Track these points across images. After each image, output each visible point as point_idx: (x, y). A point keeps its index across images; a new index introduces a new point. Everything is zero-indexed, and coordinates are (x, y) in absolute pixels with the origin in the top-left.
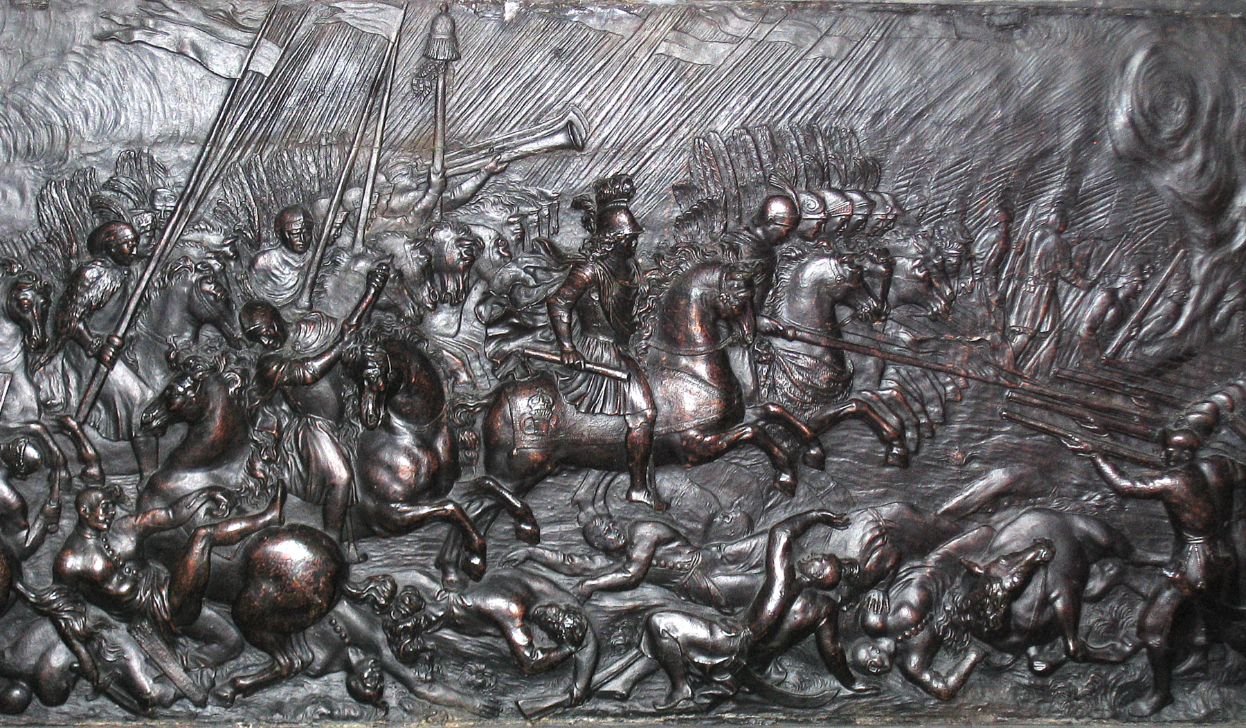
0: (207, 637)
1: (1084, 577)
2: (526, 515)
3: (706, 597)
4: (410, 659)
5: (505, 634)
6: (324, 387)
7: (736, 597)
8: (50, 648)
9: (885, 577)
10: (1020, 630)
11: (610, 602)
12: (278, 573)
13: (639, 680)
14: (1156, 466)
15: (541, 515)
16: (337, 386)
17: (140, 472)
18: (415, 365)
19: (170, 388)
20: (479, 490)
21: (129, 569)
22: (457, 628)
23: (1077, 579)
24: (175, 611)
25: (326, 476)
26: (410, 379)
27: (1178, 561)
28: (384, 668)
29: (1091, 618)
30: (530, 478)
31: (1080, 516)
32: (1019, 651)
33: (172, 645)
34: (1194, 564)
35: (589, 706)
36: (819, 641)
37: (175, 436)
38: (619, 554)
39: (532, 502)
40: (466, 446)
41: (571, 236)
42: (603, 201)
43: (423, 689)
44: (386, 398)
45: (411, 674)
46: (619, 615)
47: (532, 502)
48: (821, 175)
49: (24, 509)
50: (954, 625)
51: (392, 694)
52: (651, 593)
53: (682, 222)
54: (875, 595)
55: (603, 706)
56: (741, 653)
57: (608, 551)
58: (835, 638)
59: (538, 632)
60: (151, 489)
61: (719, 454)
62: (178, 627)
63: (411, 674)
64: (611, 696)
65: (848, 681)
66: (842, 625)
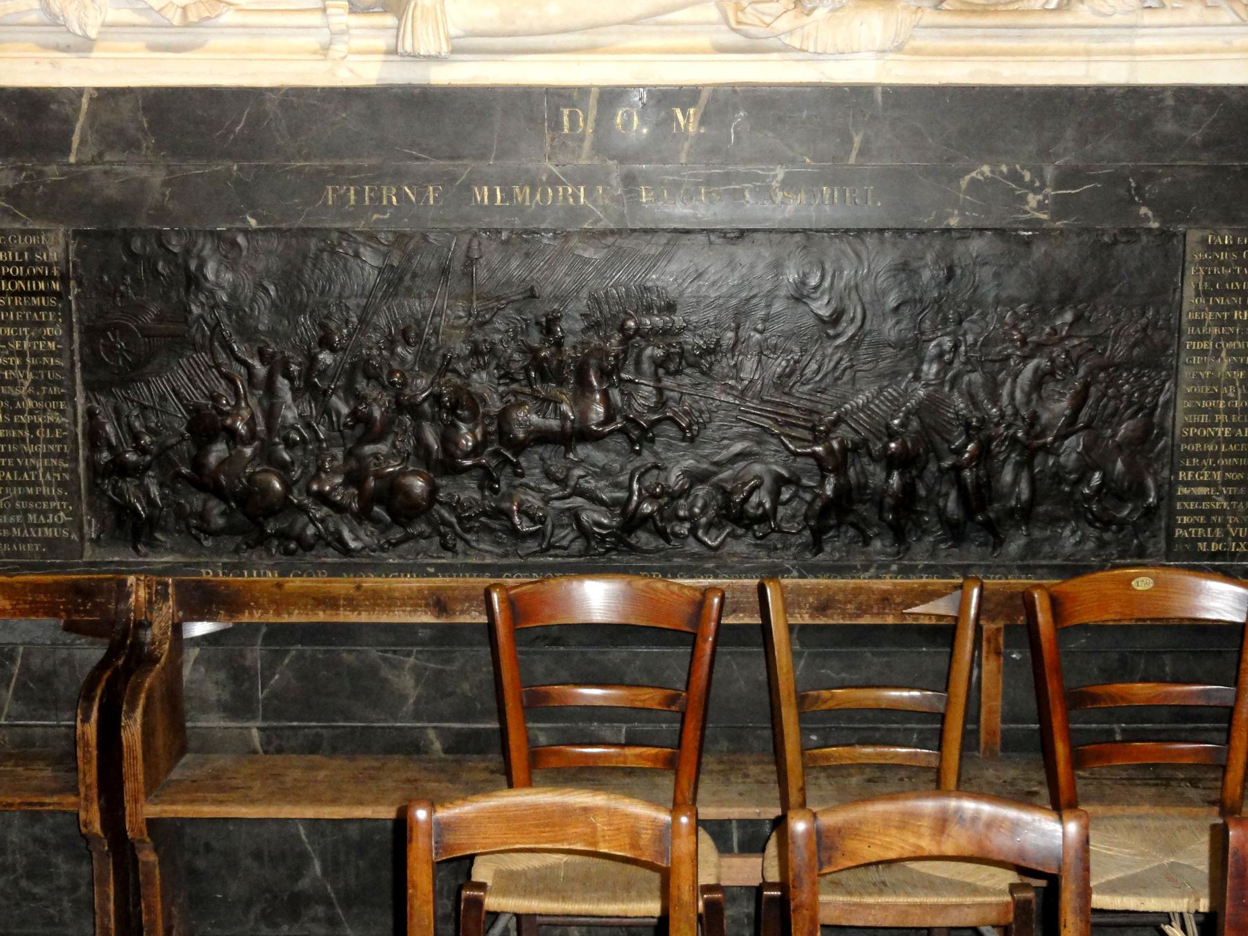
0: (376, 521)
1: (779, 493)
2: (517, 465)
3: (601, 502)
4: (468, 531)
5: (511, 519)
6: (426, 405)
7: (615, 503)
8: (306, 525)
9: (684, 493)
10: (748, 518)
11: (557, 504)
12: (407, 492)
13: (572, 541)
14: (808, 441)
15: (524, 464)
16: (431, 406)
17: (344, 446)
18: (465, 397)
19: (356, 408)
20: (496, 454)
21: (341, 490)
22: (490, 517)
23: (775, 495)
24: (361, 508)
25: (428, 448)
26: (463, 403)
27: (822, 485)
28: (457, 534)
29: (781, 511)
30: (519, 447)
31: (297, 880)
32: (748, 528)
33: (360, 524)
34: (829, 490)
35: (552, 552)
36: (655, 523)
37: (359, 430)
38: (563, 482)
39: (522, 459)
40: (490, 434)
41: (535, 338)
42: (548, 321)
43: (474, 544)
44: (452, 410)
45: (468, 537)
46: (563, 511)
47: (522, 459)
48: (648, 309)
49: (293, 463)
50: (717, 515)
51: (460, 546)
52: (578, 501)
53: (585, 331)
54: (682, 501)
55: (557, 552)
56: (618, 528)
57: (557, 481)
58: (662, 520)
59: (525, 519)
60: (349, 454)
61: (1103, 818)
62: (363, 515)
63: (468, 537)
64: (559, 547)
65: (668, 541)
66: (665, 515)
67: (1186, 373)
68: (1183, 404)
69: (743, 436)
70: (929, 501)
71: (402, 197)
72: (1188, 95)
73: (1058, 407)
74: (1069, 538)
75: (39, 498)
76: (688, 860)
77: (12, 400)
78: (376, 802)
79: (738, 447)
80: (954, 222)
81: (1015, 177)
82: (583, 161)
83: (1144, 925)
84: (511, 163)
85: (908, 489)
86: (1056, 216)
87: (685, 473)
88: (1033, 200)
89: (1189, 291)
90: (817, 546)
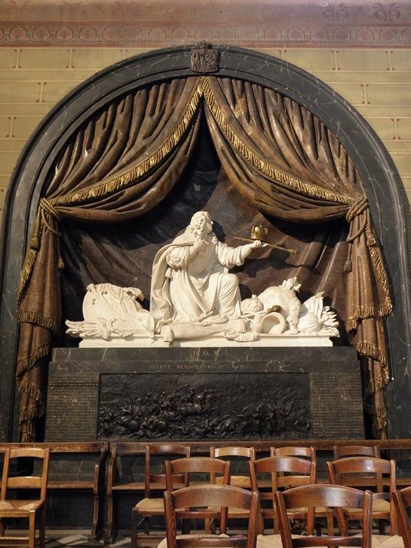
29: (237, 429)
67: (312, 400)
68: (312, 406)
69: (227, 414)
70: (265, 426)
71: (164, 367)
72: (307, 348)
73: (288, 407)
74: (293, 434)
75: (89, 427)
76: (237, 97)
77: (86, 407)
78: (335, 304)
79: (227, 416)
80: (266, 371)
81: (277, 363)
82: (197, 360)
83: (277, 480)
84: (183, 361)
85: (260, 424)
86: (285, 370)
87: (217, 421)
88: (280, 367)
89: (311, 384)
90: (244, 436)
